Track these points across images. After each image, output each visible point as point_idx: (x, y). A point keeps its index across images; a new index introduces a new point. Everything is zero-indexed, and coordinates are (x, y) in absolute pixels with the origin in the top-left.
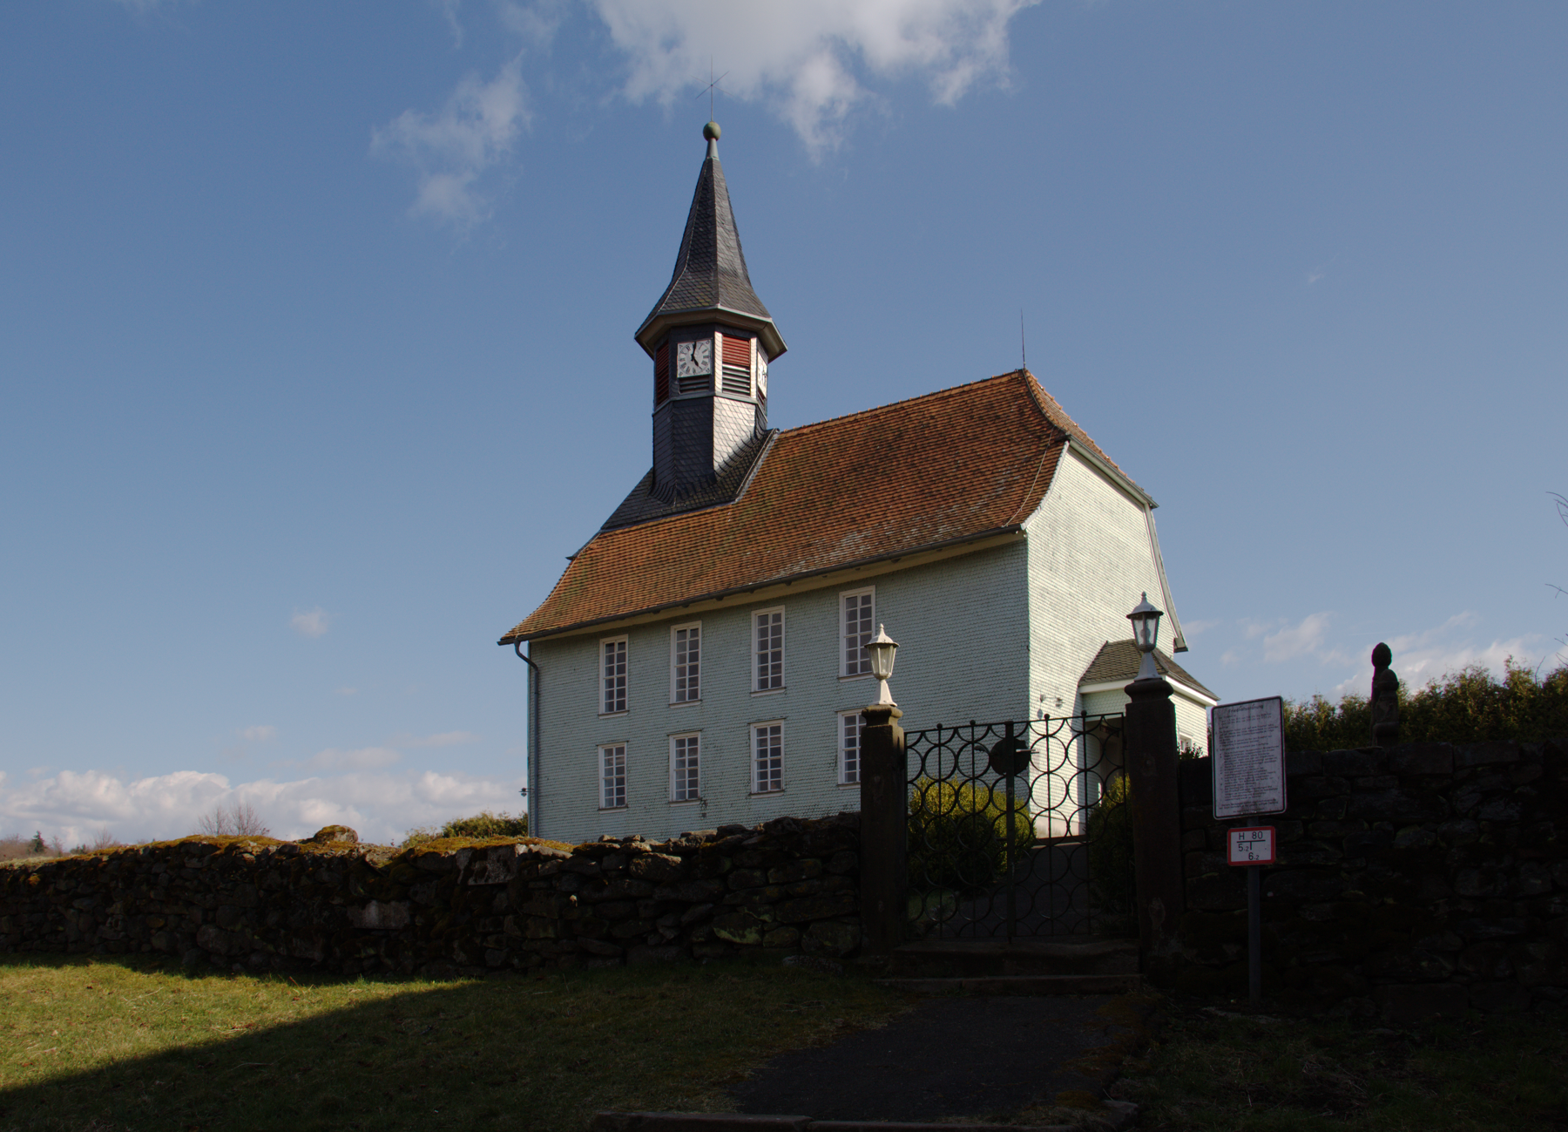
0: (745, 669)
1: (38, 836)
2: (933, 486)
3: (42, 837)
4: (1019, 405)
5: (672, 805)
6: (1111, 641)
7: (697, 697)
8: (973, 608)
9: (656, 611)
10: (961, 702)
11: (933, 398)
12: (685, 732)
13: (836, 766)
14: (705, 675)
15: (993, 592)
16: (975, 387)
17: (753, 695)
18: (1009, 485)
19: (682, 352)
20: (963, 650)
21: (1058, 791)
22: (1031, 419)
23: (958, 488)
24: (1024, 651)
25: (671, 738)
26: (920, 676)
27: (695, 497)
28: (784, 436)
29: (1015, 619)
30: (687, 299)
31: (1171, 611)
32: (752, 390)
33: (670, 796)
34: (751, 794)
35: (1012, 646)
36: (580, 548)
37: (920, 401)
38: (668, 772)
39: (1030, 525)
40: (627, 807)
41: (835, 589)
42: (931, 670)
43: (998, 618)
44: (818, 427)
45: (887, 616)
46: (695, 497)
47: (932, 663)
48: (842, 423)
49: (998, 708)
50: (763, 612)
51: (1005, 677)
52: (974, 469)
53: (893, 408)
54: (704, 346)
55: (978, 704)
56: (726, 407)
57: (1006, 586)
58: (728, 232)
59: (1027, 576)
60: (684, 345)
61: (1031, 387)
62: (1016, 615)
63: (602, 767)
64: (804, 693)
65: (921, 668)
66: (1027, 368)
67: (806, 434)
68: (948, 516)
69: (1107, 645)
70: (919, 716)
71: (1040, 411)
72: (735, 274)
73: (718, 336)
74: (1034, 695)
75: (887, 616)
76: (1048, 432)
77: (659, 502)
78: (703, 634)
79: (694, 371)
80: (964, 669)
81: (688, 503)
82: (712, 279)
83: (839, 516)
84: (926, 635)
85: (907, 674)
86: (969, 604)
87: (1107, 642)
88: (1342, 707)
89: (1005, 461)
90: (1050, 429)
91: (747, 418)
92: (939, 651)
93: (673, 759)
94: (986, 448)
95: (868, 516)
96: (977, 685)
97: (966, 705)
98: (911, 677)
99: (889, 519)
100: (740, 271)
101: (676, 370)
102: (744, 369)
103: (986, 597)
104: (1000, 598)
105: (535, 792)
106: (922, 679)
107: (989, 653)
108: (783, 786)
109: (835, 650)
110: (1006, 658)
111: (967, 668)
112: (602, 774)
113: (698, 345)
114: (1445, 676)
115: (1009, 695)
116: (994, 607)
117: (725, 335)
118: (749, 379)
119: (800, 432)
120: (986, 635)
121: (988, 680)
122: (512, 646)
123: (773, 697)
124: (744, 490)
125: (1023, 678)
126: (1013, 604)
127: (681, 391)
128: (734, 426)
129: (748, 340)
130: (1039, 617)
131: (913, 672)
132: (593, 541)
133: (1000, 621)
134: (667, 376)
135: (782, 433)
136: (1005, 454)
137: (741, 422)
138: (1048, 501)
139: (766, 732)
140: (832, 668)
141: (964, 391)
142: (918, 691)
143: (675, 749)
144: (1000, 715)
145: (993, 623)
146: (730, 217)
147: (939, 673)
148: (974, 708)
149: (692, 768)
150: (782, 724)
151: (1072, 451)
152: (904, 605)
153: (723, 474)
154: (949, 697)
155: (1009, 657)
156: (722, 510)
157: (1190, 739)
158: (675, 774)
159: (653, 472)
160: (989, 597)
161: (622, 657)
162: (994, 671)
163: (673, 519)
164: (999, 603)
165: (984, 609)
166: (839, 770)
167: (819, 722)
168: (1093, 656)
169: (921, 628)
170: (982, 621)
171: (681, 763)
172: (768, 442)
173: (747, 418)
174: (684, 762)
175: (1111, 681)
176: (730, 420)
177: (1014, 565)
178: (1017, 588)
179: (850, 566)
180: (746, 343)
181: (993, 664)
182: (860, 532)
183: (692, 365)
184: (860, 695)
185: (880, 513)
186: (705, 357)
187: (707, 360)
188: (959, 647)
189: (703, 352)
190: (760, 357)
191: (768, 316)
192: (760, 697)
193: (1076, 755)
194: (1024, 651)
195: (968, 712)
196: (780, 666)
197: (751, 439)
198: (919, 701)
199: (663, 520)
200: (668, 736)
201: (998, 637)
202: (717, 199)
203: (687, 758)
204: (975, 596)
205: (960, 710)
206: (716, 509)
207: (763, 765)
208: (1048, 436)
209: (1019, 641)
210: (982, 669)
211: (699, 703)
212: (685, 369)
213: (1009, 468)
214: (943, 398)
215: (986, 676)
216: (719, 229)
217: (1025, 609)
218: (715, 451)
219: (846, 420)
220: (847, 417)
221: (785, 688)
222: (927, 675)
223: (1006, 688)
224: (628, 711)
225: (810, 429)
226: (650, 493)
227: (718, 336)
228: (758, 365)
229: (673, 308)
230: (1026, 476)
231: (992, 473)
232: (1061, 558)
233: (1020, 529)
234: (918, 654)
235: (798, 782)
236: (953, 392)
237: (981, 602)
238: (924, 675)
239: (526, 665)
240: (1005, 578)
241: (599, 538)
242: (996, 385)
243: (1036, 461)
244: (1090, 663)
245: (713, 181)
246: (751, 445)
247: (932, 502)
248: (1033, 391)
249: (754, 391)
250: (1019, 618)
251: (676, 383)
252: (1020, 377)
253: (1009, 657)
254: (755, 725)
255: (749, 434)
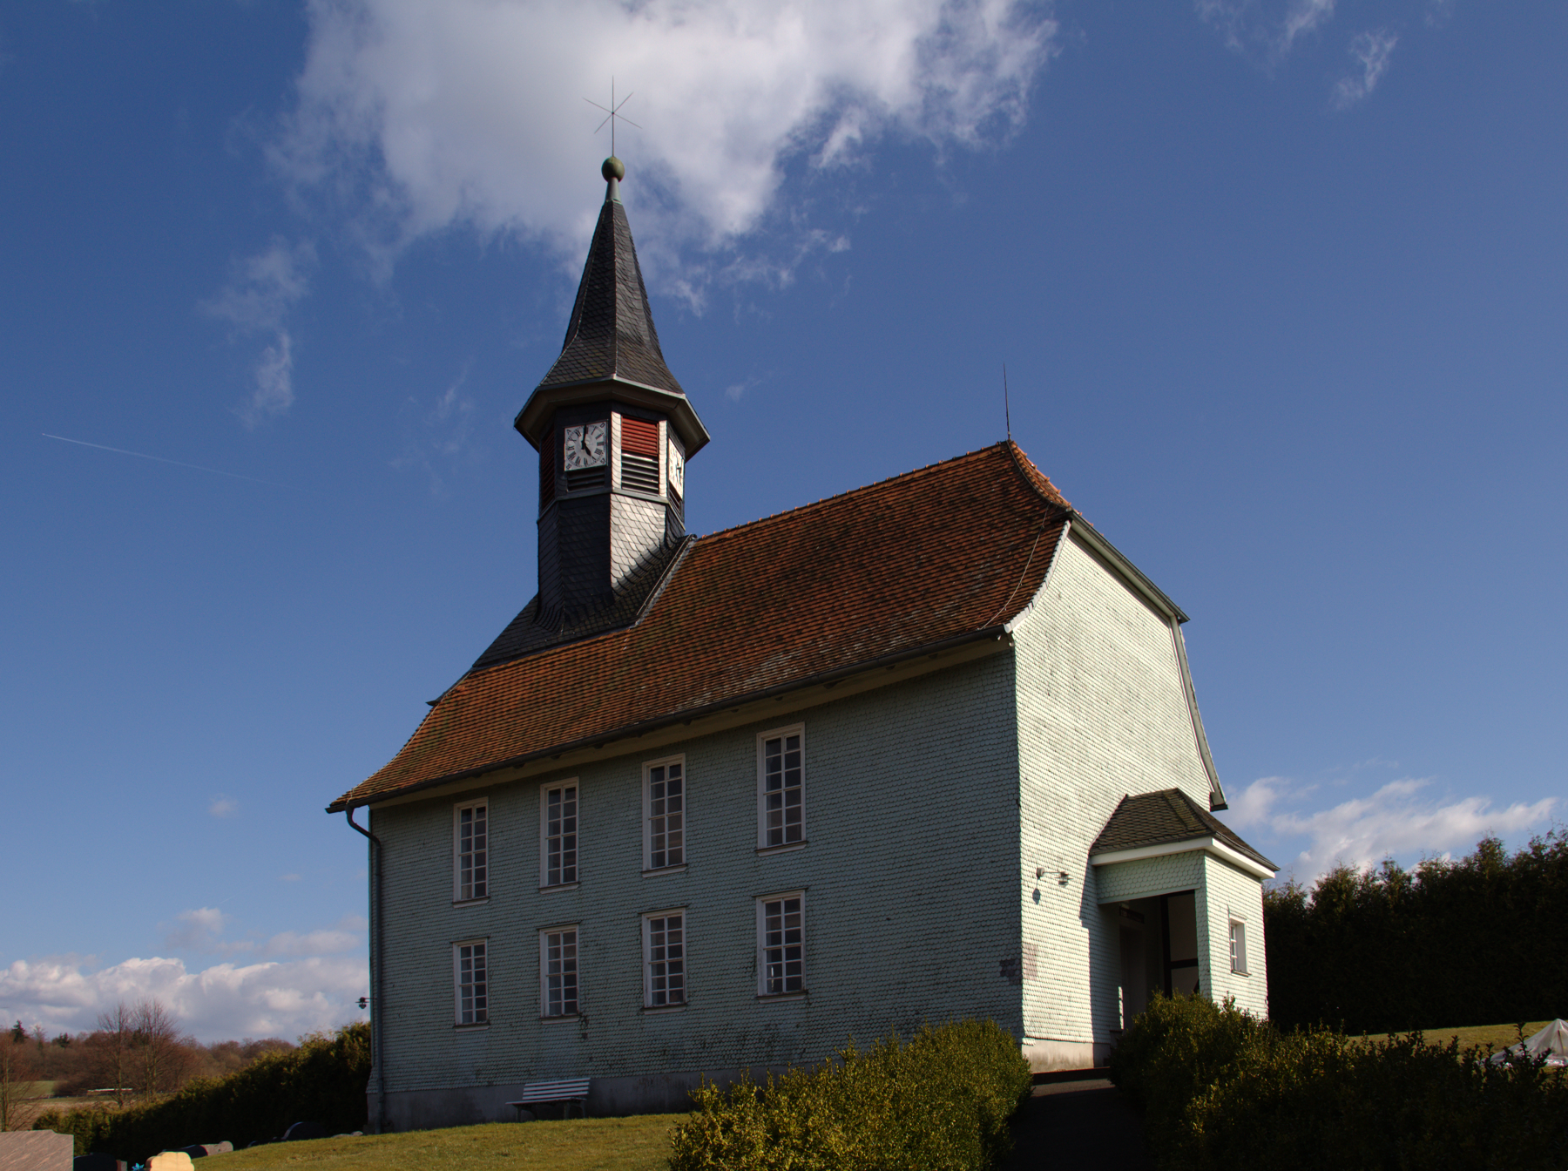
0: (634, 840)
1: (19, 1026)
2: (886, 590)
3: (22, 1026)
4: (1002, 484)
5: (544, 1022)
6: (1132, 794)
7: (574, 879)
8: (940, 748)
9: (518, 763)
10: (924, 882)
11: (891, 484)
12: (558, 925)
13: (754, 971)
14: (583, 849)
15: (967, 726)
16: (945, 466)
17: (645, 876)
18: (989, 580)
19: (570, 439)
20: (926, 808)
21: (1063, 1003)
22: (1019, 498)
23: (920, 589)
24: (1012, 808)
25: (542, 933)
26: (868, 845)
27: (587, 622)
28: (701, 543)
29: (999, 762)
30: (575, 370)
31: (1206, 757)
32: (661, 486)
33: (542, 1010)
34: (643, 1009)
35: (996, 800)
36: (445, 690)
37: (874, 489)
38: (538, 977)
39: (1018, 627)
40: (489, 1024)
41: (752, 729)
42: (883, 837)
43: (975, 761)
44: (744, 530)
45: (821, 764)
46: (587, 622)
47: (883, 827)
48: (774, 523)
49: (977, 888)
50: (657, 763)
51: (985, 845)
52: (941, 564)
53: (839, 500)
54: (598, 430)
55: (948, 883)
56: (626, 507)
57: (985, 716)
58: (632, 290)
59: (1014, 701)
60: (573, 429)
61: (1018, 460)
62: (1000, 757)
63: (458, 971)
64: (711, 871)
65: (868, 834)
66: (1011, 439)
67: (729, 539)
68: (904, 625)
69: (1126, 799)
70: (867, 901)
71: (1031, 488)
72: (640, 342)
73: (616, 419)
74: (1027, 869)
75: (821, 764)
76: (1042, 512)
77: (544, 631)
78: (580, 794)
79: (586, 462)
80: (928, 834)
81: (577, 630)
82: (608, 345)
83: (762, 635)
84: (875, 788)
85: (849, 843)
86: (934, 744)
87: (1127, 795)
88: (1419, 875)
89: (984, 551)
90: (1045, 508)
91: (655, 522)
92: (892, 810)
94: (957, 538)
95: (800, 632)
96: (947, 857)
97: (931, 885)
98: (855, 847)
99: (826, 633)
100: (646, 339)
101: (564, 461)
102: (651, 460)
103: (957, 733)
104: (977, 734)
106: (870, 850)
107: (963, 811)
108: (686, 999)
110: (986, 818)
111: (931, 833)
112: (458, 980)
113: (590, 429)
114: (1550, 834)
115: (992, 870)
116: (968, 747)
117: (624, 416)
118: (658, 472)
119: (721, 537)
120: (958, 786)
121: (961, 849)
122: (343, 814)
123: (671, 878)
124: (646, 610)
125: (1012, 845)
126: (996, 741)
127: (570, 489)
128: (637, 532)
129: (656, 424)
130: (1032, 759)
131: (857, 841)
132: (461, 682)
133: (977, 766)
135: (700, 540)
136: (984, 543)
137: (647, 527)
138: (1042, 597)
139: (663, 926)
140: (749, 837)
141: (930, 473)
142: (864, 866)
143: (547, 947)
144: (979, 899)
145: (968, 768)
146: (634, 273)
147: (894, 840)
148: (942, 889)
149: (569, 972)
150: (683, 913)
151: (1075, 536)
152: (843, 748)
153: (623, 592)
154: (907, 874)
155: (991, 817)
156: (618, 636)
157: (1243, 924)
158: (547, 980)
159: (539, 597)
160: (962, 732)
161: (481, 828)
162: (970, 837)
163: (558, 650)
164: (975, 740)
165: (954, 750)
166: (759, 977)
167: (732, 910)
168: (1109, 814)
169: (867, 779)
170: (952, 766)
172: (681, 551)
173: (655, 522)
175: (1135, 848)
176: (632, 524)
177: (996, 686)
178: (1001, 719)
179: (768, 694)
180: (653, 427)
181: (969, 826)
182: (786, 652)
183: (582, 455)
184: (786, 873)
185: (815, 628)
186: (599, 444)
187: (601, 448)
188: (920, 804)
189: (597, 438)
190: (672, 446)
191: (681, 392)
192: (655, 877)
193: (1088, 950)
194: (1012, 808)
195: (935, 895)
197: (661, 548)
198: (865, 881)
199: (547, 653)
200: (538, 930)
201: (975, 788)
202: (617, 250)
204: (941, 732)
205: (923, 892)
206: (611, 636)
207: (659, 969)
208: (1042, 516)
209: (1004, 793)
210: (954, 835)
211: (576, 887)
213: (989, 560)
214: (903, 483)
215: (958, 844)
216: (620, 286)
217: (1013, 748)
218: (613, 564)
219: (780, 519)
220: (781, 515)
221: (687, 865)
222: (877, 844)
223: (988, 861)
224: (489, 897)
225: (734, 532)
226: (534, 621)
227: (616, 419)
228: (671, 460)
229: (557, 382)
230: (1012, 567)
231: (966, 568)
232: (1063, 678)
233: (1002, 631)
234: (864, 815)
235: (704, 993)
236: (916, 475)
237: (951, 740)
238: (872, 844)
239: (365, 840)
240: (984, 706)
241: (469, 678)
242: (971, 463)
243: (1026, 549)
244: (1105, 824)
245: (613, 228)
246: (660, 556)
247: (884, 609)
248: (1021, 465)
249: (663, 487)
250: (1004, 761)
251: (563, 478)
252: (1004, 451)
253: (991, 817)
254: (547, 931)
255: (657, 542)
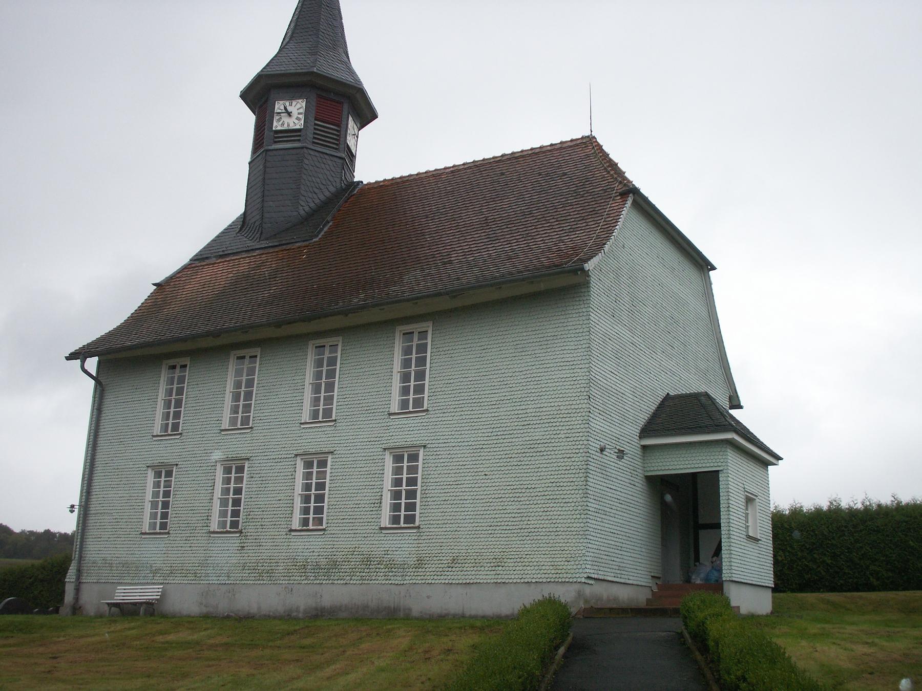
9: (184, 340)
47: (486, 404)
77: (245, 239)
87: (714, 268)
93: (219, 486)
97: (519, 451)
105: (85, 510)
109: (388, 385)
129: (341, 103)
134: (264, 129)
142: (469, 432)
145: (552, 365)
154: (501, 441)
159: (245, 213)
167: (367, 458)
171: (226, 491)
174: (228, 489)
186: (299, 114)
196: (332, 397)
201: (556, 380)
203: (232, 485)
209: (578, 386)
212: (280, 123)
233: (583, 269)
250: (579, 362)
